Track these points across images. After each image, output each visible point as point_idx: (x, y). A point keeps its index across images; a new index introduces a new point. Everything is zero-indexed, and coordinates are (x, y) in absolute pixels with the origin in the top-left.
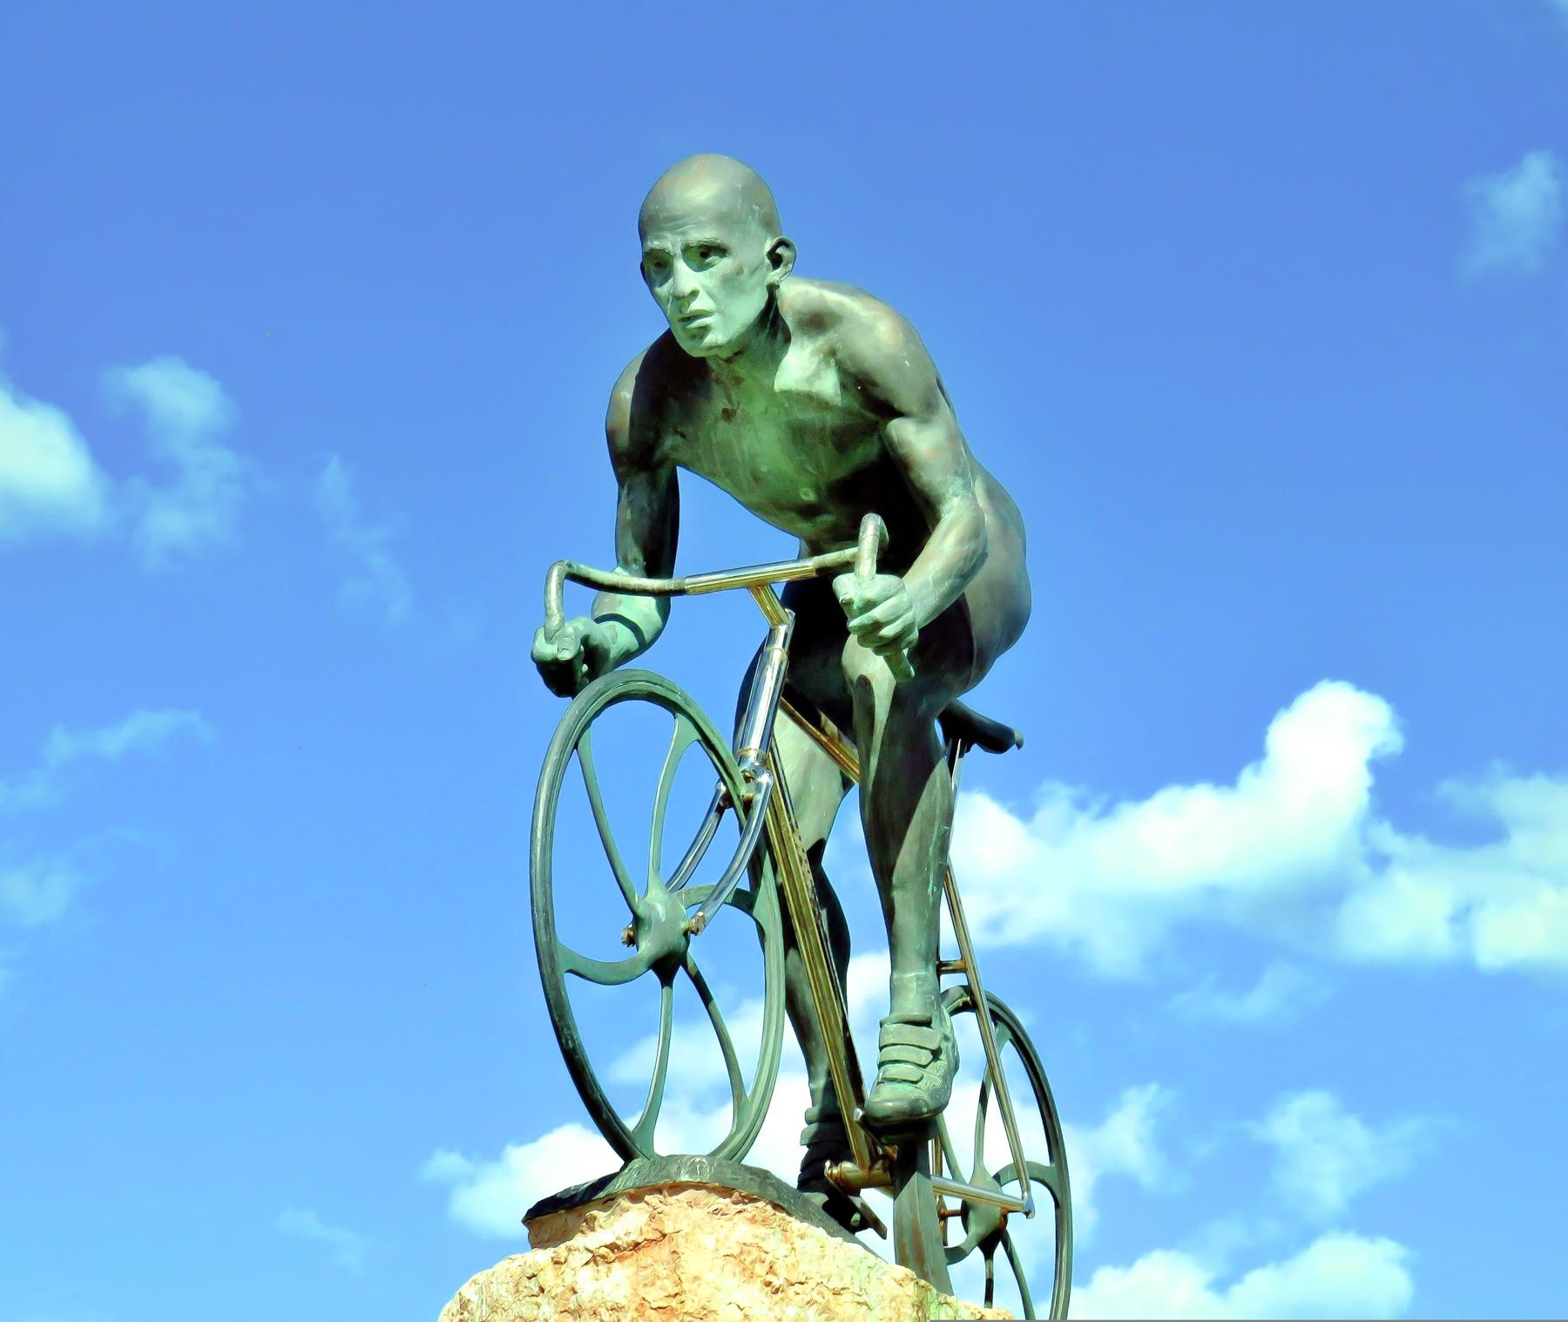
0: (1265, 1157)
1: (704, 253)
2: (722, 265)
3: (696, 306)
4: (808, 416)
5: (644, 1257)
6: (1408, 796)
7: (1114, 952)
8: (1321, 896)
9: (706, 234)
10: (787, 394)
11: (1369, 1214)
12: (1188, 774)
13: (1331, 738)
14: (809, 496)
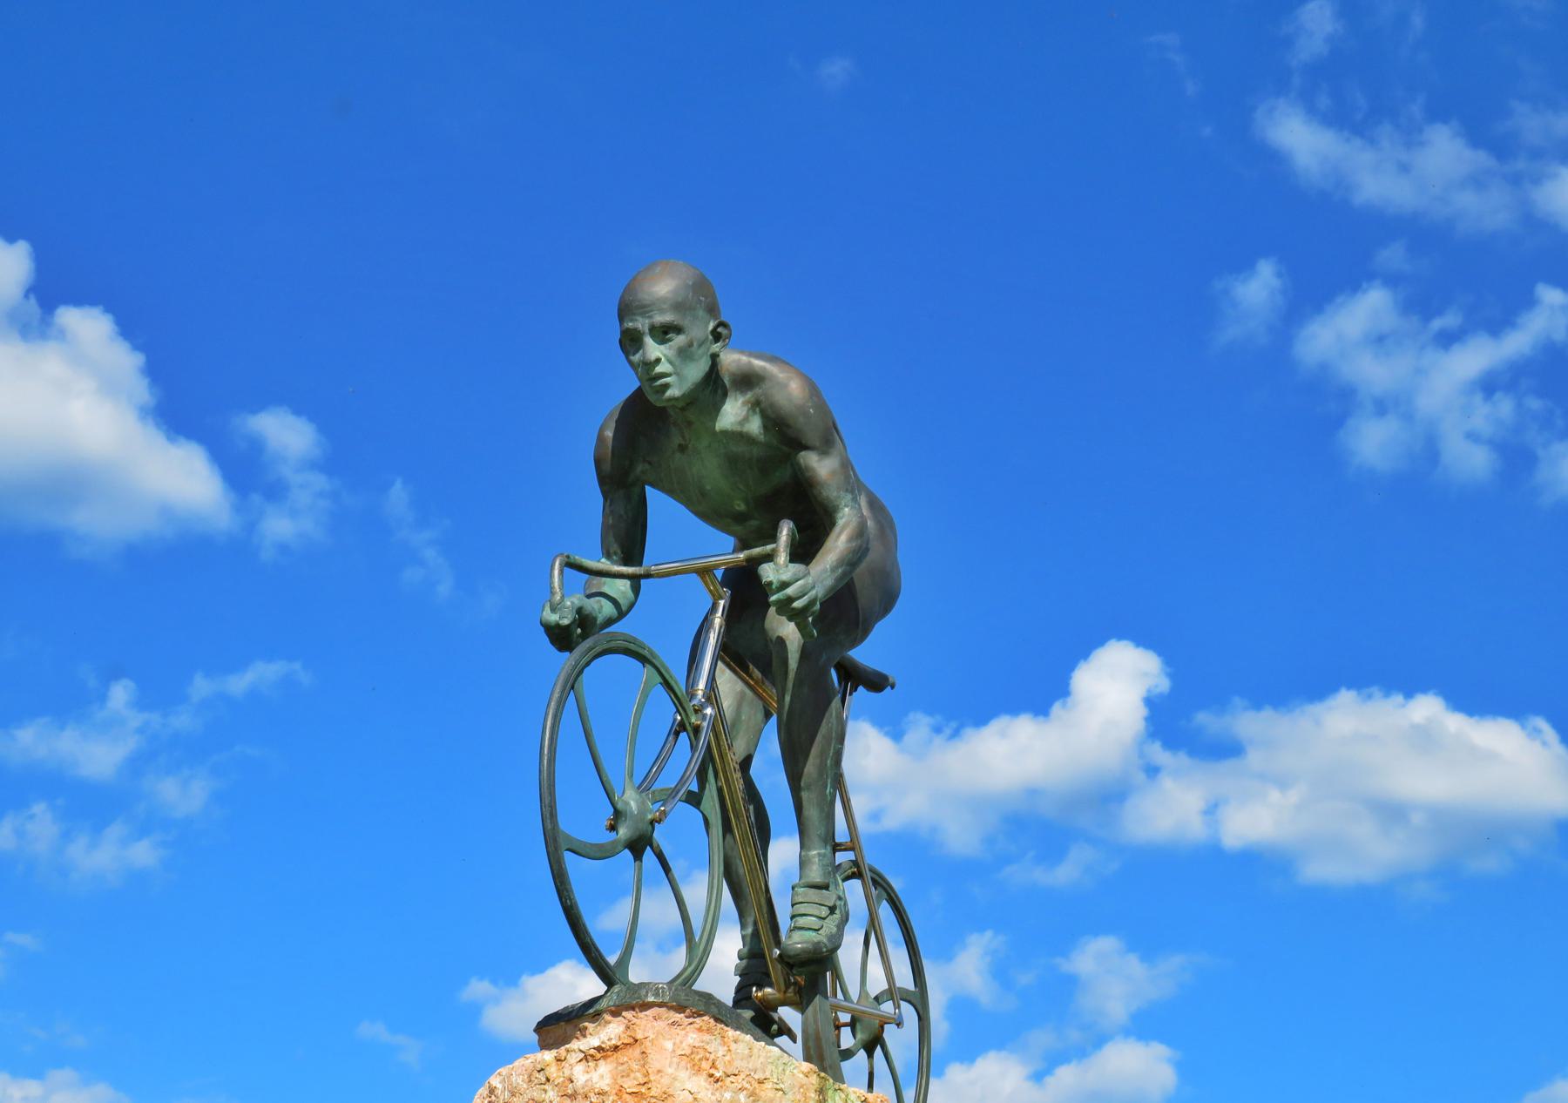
0: (1070, 984)
2: (680, 340)
3: (659, 369)
5: (622, 1056)
6: (1170, 723)
8: (1107, 796)
9: (660, 319)
10: (725, 433)
13: (1115, 685)
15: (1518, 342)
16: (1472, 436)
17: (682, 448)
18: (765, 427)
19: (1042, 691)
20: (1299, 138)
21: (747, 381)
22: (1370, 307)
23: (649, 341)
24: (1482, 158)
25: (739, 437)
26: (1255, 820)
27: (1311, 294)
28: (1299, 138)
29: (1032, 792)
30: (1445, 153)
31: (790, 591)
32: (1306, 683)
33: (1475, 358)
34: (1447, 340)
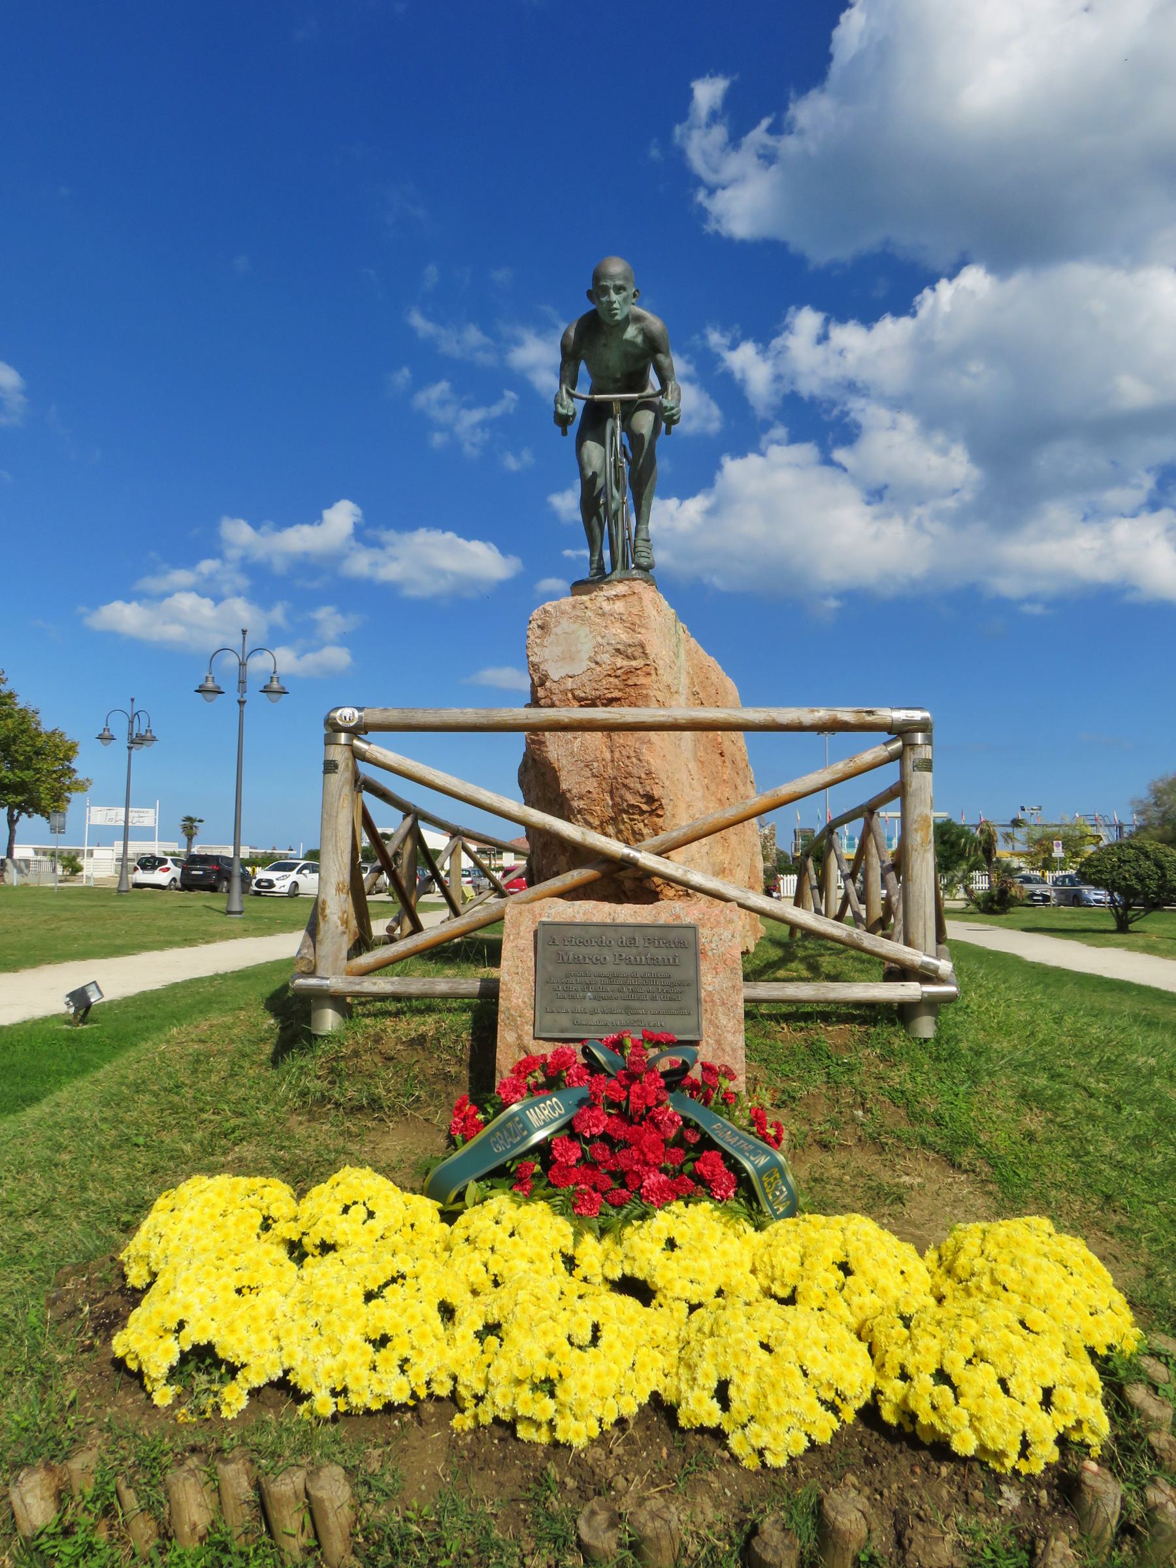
0: (314, 624)
1: (619, 289)
2: (624, 294)
3: (615, 306)
4: (630, 349)
5: (629, 599)
6: (362, 535)
7: (279, 566)
8: (336, 558)
9: (619, 283)
10: (626, 341)
11: (344, 640)
12: (303, 521)
13: (341, 518)
14: (619, 375)
15: (497, 410)
16: (473, 445)
17: (605, 345)
18: (644, 341)
19: (314, 517)
20: (418, 321)
21: (638, 319)
22: (441, 388)
23: (612, 291)
24: (486, 340)
25: (631, 343)
26: (391, 572)
27: (422, 381)
28: (418, 321)
29: (306, 554)
30: (473, 335)
31: (674, 411)
32: (409, 523)
33: (476, 415)
34: (469, 406)
